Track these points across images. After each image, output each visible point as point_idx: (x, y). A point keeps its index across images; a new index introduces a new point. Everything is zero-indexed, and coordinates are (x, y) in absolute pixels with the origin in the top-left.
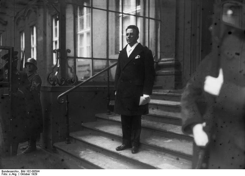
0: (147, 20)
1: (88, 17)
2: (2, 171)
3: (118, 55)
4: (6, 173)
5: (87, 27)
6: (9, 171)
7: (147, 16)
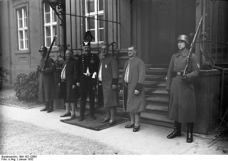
0: (115, 20)
1: (25, 20)
2: (2, 157)
3: (100, 59)
4: (6, 158)
5: (25, 27)
6: (8, 157)
7: (82, 18)
